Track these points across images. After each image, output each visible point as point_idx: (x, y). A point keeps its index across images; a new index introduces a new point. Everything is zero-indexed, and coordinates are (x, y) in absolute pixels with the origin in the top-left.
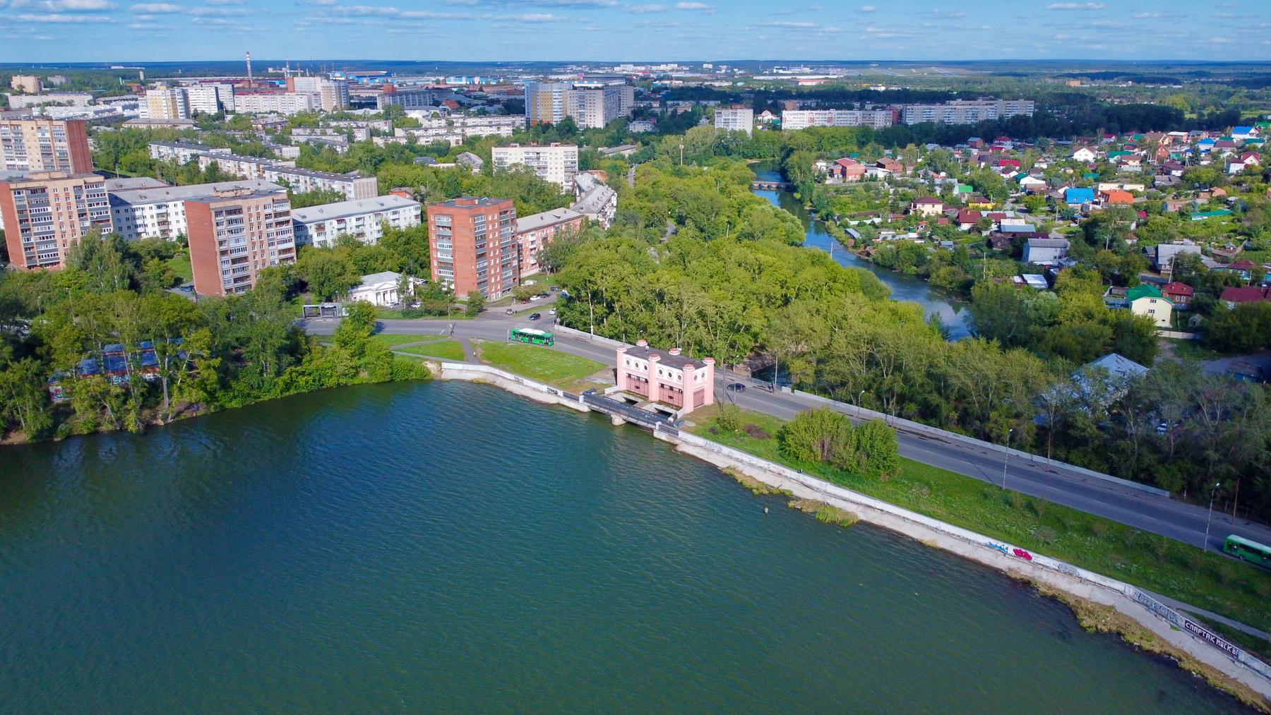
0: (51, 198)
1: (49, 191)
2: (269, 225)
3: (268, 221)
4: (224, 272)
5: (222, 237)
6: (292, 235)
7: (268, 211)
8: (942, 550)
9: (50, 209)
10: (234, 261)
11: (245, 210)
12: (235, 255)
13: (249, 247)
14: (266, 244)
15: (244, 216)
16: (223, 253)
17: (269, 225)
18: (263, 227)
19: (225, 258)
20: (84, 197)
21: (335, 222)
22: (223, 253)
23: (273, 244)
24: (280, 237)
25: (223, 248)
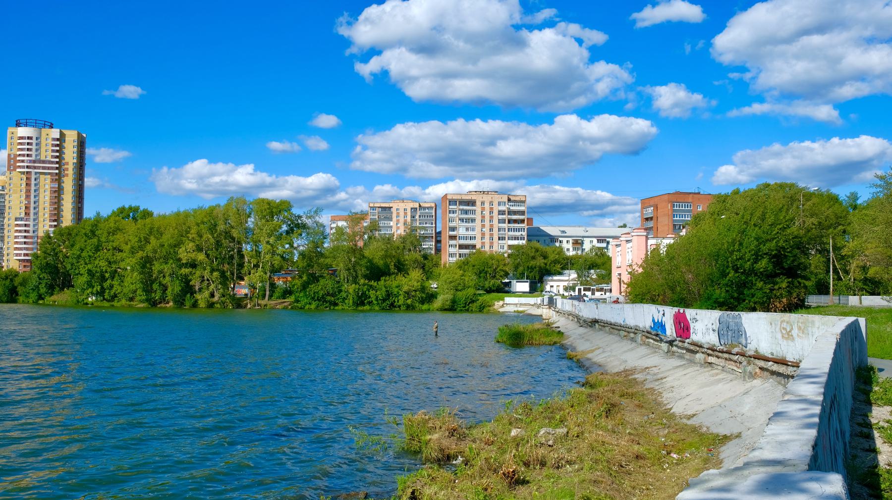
0: (394, 215)
1: (394, 210)
2: (503, 221)
3: (501, 217)
4: (451, 255)
5: (452, 224)
6: (525, 234)
7: (502, 208)
8: (835, 353)
9: (392, 224)
10: (461, 247)
11: (478, 203)
12: (462, 242)
13: (479, 236)
14: (496, 237)
15: (478, 208)
16: (453, 238)
17: (503, 221)
18: (495, 221)
19: (453, 242)
20: (417, 217)
21: (595, 240)
22: (453, 238)
23: (503, 239)
24: (511, 233)
25: (452, 233)
